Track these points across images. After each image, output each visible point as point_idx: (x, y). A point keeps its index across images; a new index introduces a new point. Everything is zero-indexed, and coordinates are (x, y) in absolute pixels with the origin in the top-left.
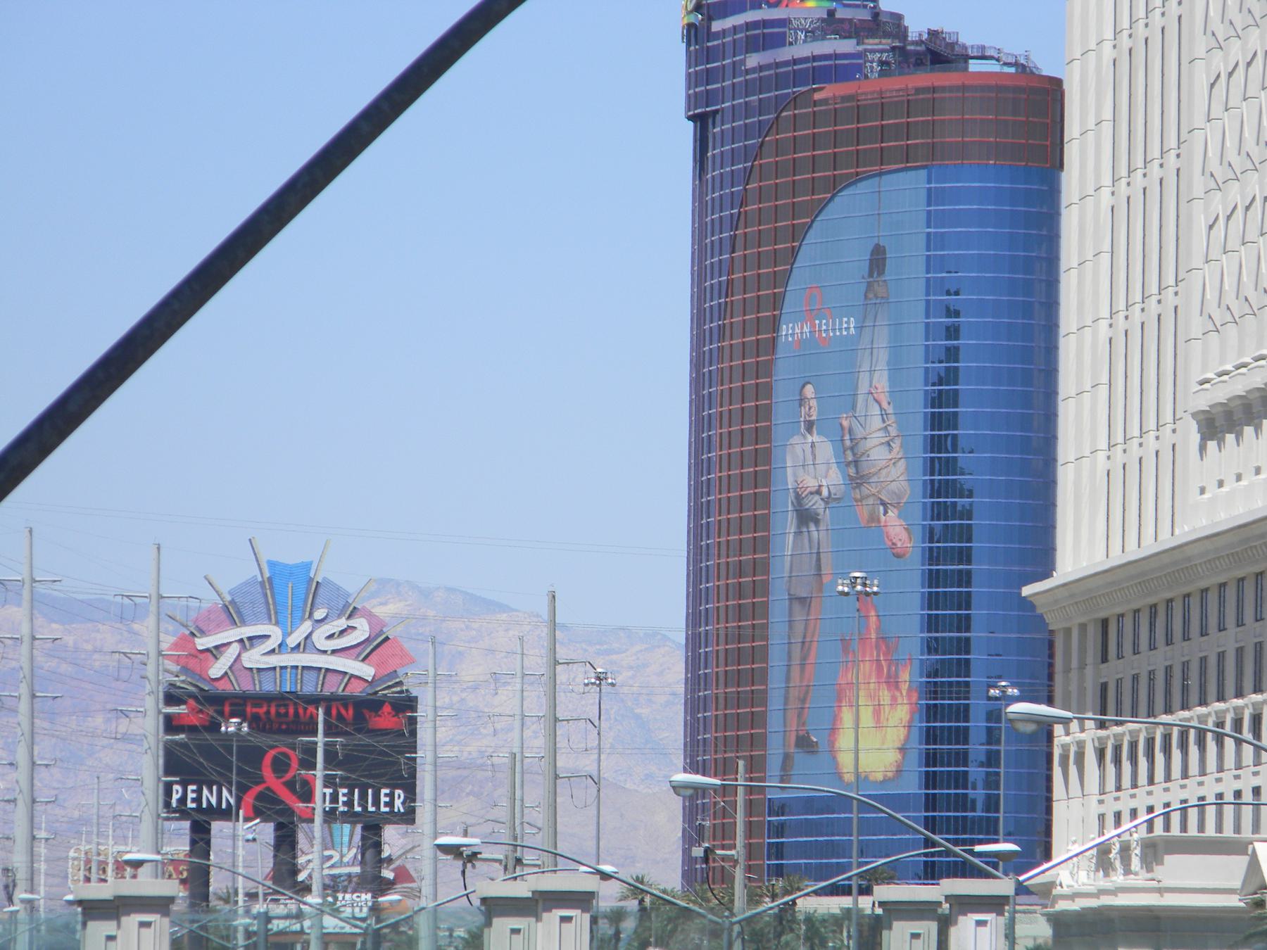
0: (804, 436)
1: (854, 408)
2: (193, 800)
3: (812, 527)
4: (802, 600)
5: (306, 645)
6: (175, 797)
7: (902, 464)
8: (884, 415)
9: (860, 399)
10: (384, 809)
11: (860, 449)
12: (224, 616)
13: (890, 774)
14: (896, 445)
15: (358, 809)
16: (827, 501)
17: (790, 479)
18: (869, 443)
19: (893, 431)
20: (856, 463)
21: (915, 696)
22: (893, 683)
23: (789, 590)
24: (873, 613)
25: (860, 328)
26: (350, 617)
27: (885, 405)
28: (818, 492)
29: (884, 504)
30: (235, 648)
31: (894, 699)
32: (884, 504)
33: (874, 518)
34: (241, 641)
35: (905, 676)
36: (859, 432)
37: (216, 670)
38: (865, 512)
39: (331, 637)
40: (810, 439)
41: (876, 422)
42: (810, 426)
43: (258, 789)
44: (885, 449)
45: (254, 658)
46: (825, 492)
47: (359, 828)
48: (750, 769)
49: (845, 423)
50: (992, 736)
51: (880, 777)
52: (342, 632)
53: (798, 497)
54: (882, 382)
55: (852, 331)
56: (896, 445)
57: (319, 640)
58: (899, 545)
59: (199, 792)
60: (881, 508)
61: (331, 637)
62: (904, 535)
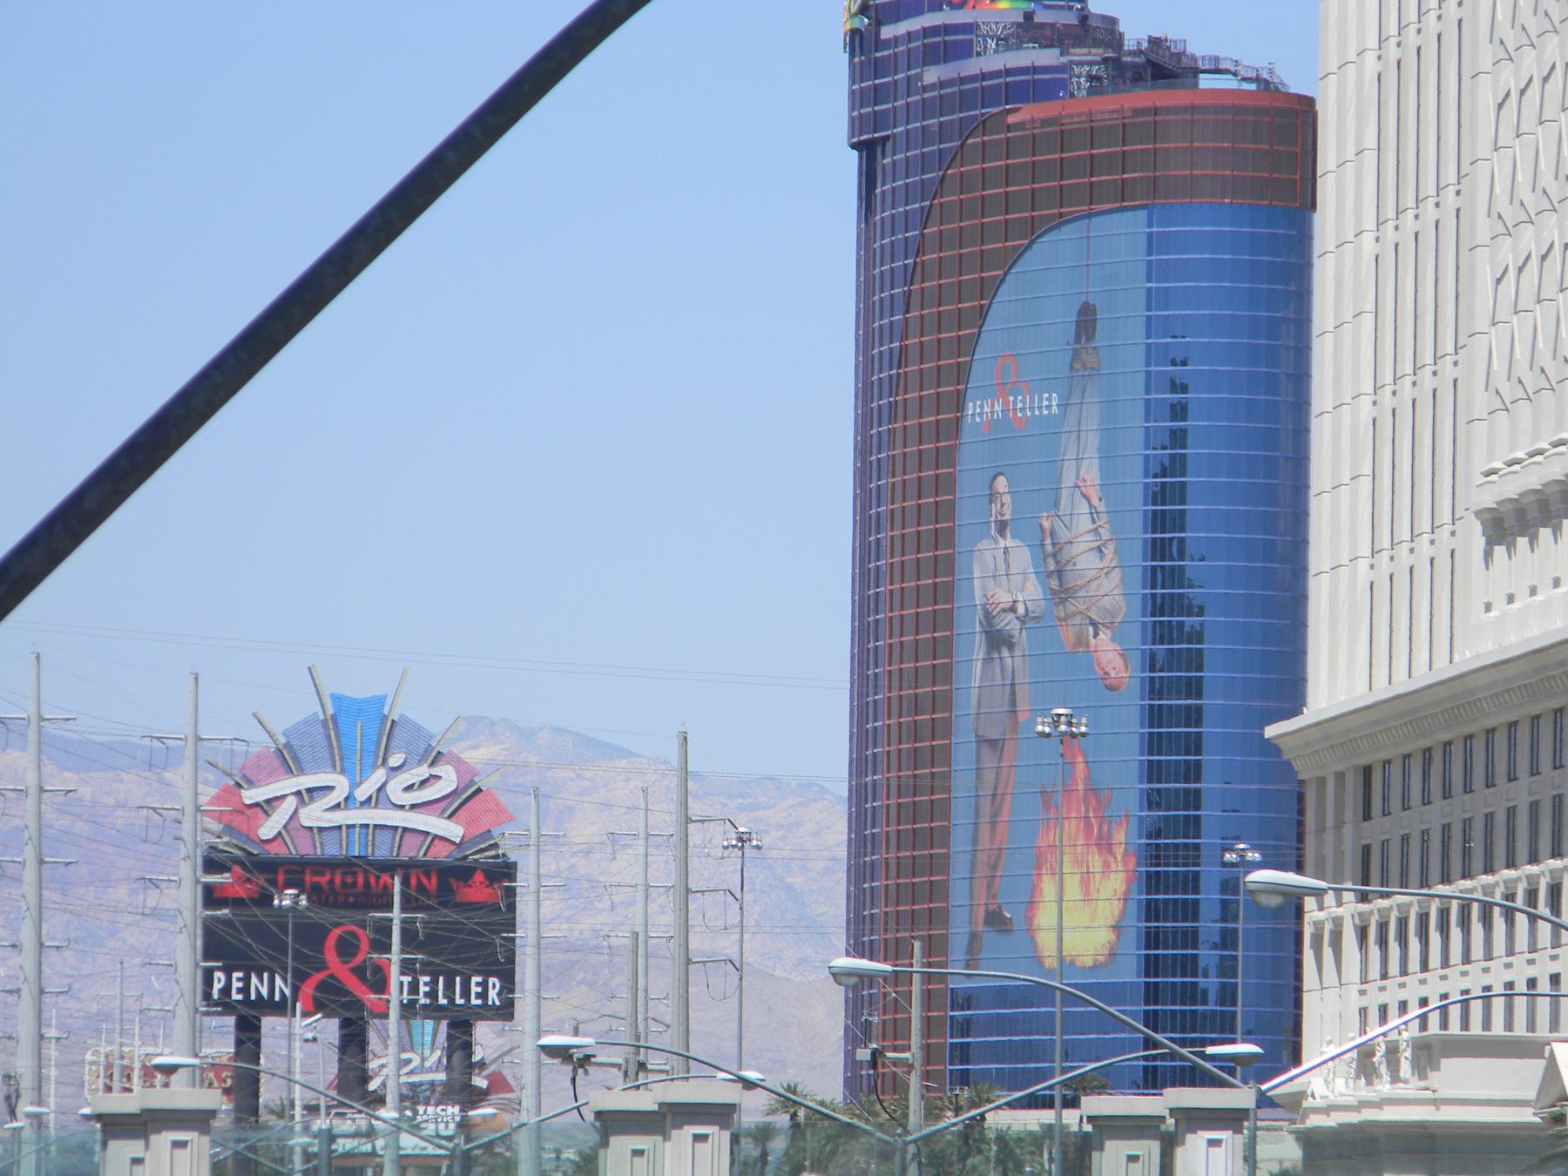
0: (995, 540)
1: (1057, 505)
2: (239, 991)
3: (1005, 653)
4: (992, 743)
5: (378, 798)
6: (217, 986)
7: (1116, 574)
8: (1094, 514)
9: (1065, 494)
10: (475, 1002)
11: (1065, 556)
12: (277, 763)
13: (1101, 959)
14: (1109, 551)
15: (443, 1001)
16: (1023, 620)
17: (978, 594)
18: (1076, 549)
19: (1105, 534)
20: (1059, 573)
21: (1132, 862)
22: (1105, 846)
23: (976, 731)
24: (1080, 759)
25: (1064, 406)
26: (433, 764)
27: (1095, 501)
28: (1013, 609)
29: (1094, 624)
30: (291, 803)
31: (1106, 865)
32: (1094, 624)
33: (1081, 641)
34: (298, 793)
35: (1120, 837)
36: (1063, 535)
37: (268, 830)
38: (1070, 634)
39: (409, 788)
40: (1002, 543)
41: (1085, 523)
42: (1002, 527)
43: (320, 976)
44: (1095, 555)
45: (314, 815)
46: (1021, 610)
47: (444, 1025)
48: (928, 952)
49: (1046, 524)
50: (1227, 911)
51: (1089, 962)
52: (423, 783)
53: (988, 615)
54: (1091, 473)
55: (1055, 409)
56: (1109, 551)
57: (395, 792)
58: (1113, 674)
59: (246, 980)
60: (1091, 629)
61: (409, 788)
62: (1119, 663)
